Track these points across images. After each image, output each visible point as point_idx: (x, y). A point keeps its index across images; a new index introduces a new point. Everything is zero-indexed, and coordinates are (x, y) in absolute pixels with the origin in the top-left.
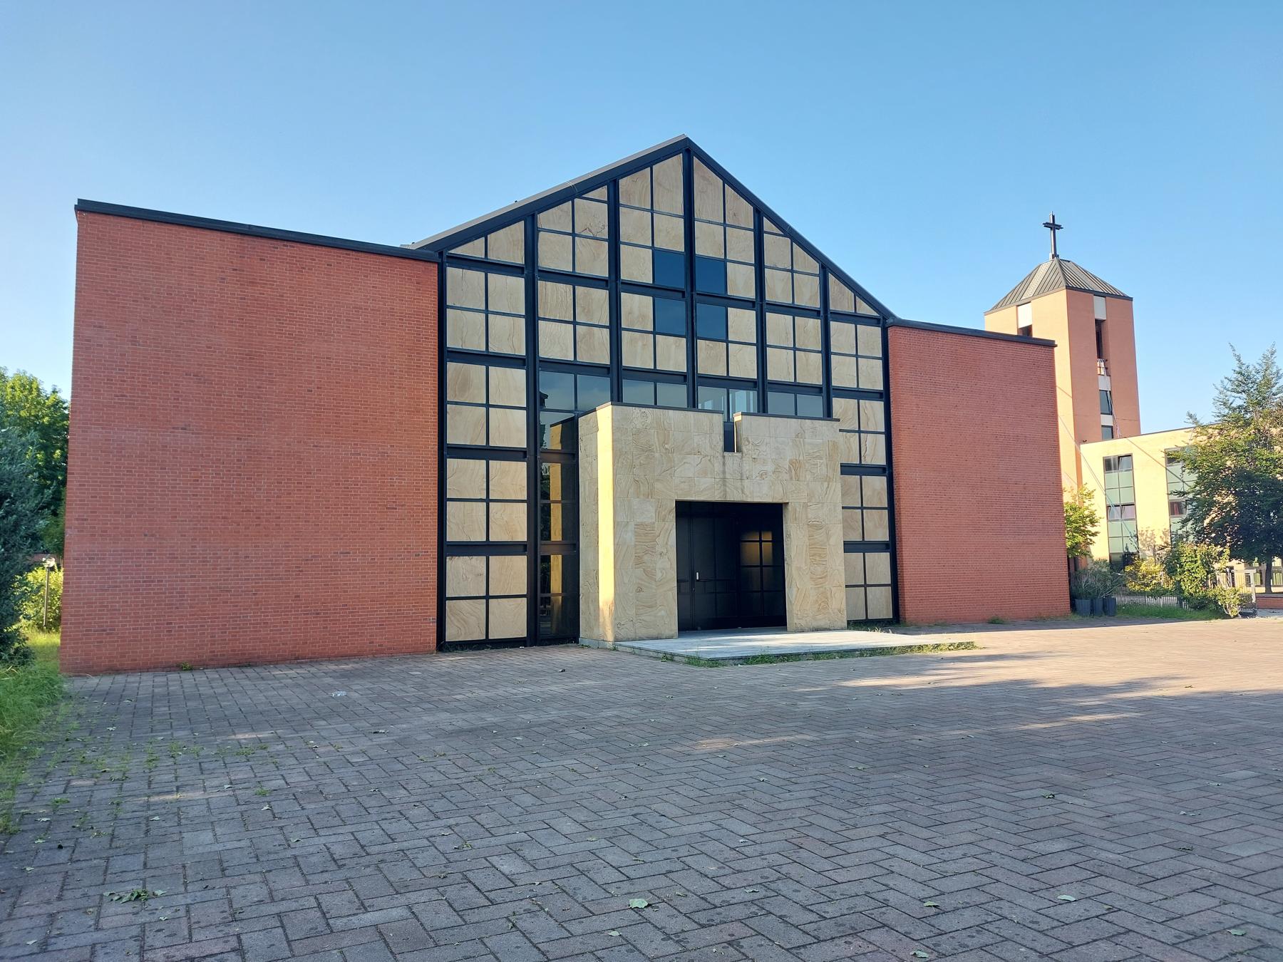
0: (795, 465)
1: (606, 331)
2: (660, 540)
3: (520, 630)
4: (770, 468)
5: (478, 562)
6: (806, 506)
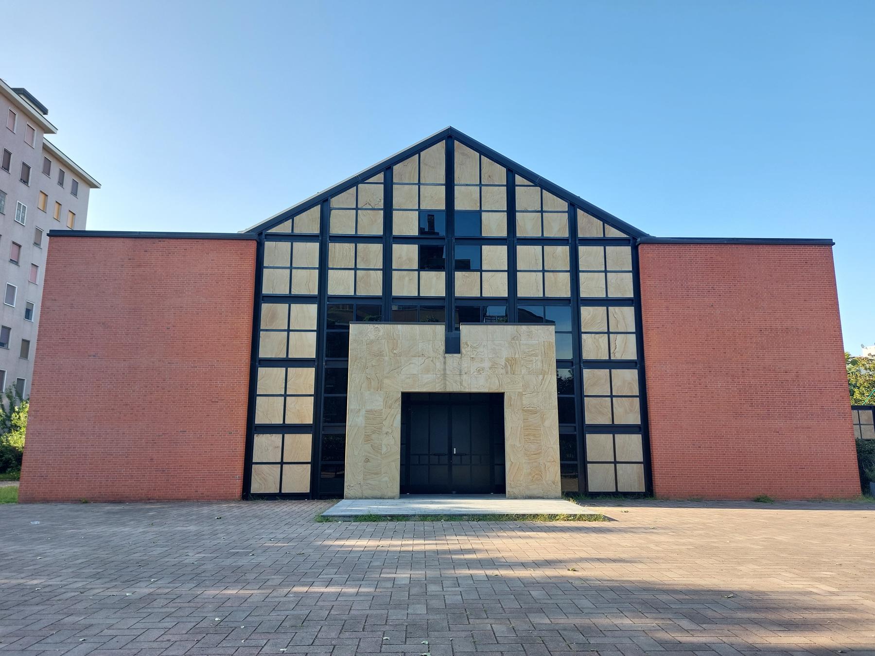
0: (511, 362)
1: (380, 273)
2: (386, 423)
3: (305, 488)
4: (487, 365)
5: (276, 438)
6: (520, 395)
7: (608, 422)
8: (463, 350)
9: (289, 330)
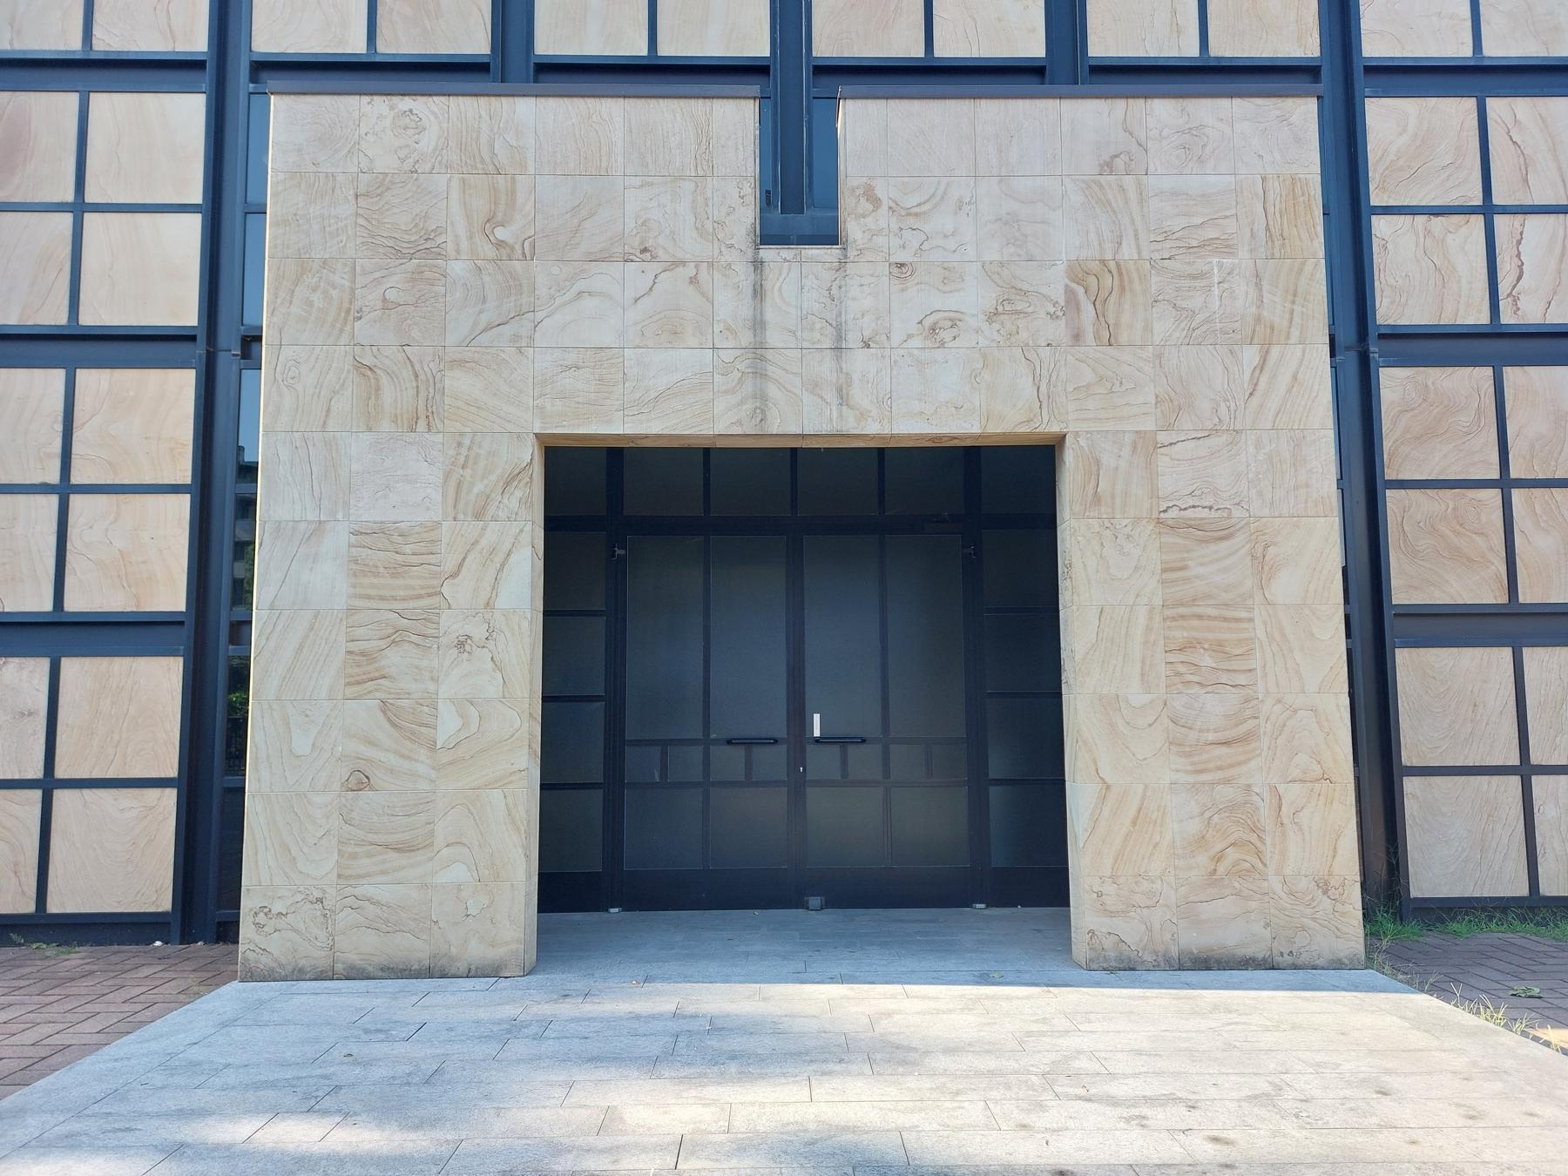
0: (1097, 290)
2: (459, 592)
4: (973, 298)
6: (1147, 447)
7: (1493, 595)
8: (852, 228)
9: (79, 208)
